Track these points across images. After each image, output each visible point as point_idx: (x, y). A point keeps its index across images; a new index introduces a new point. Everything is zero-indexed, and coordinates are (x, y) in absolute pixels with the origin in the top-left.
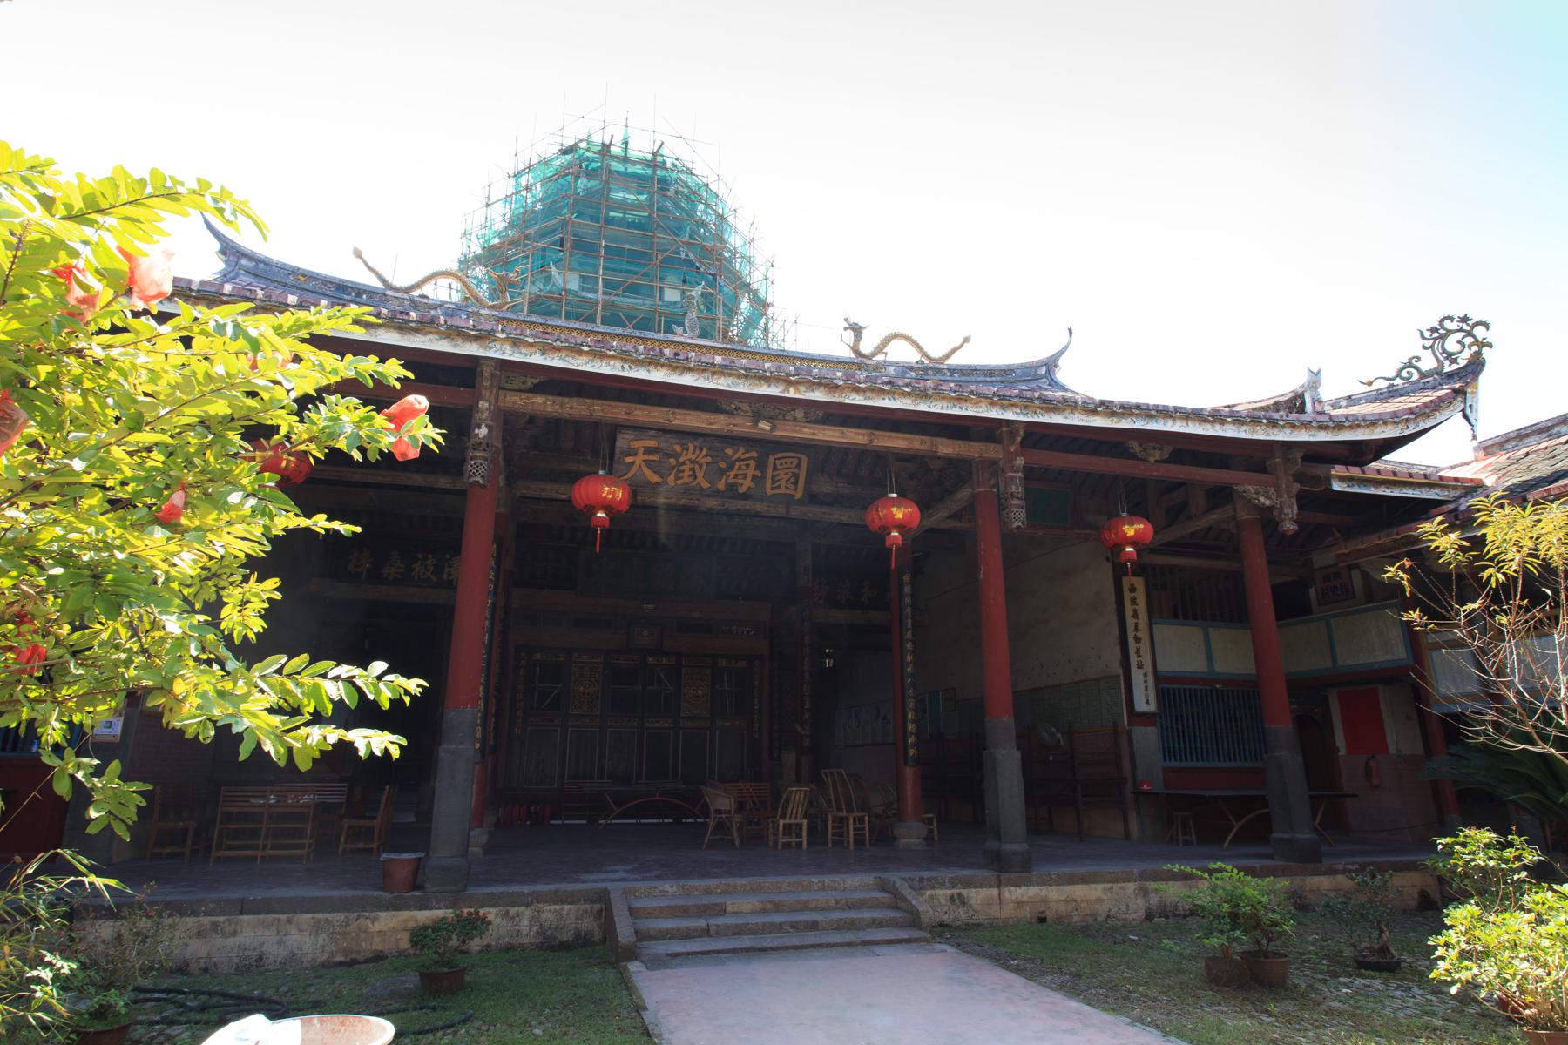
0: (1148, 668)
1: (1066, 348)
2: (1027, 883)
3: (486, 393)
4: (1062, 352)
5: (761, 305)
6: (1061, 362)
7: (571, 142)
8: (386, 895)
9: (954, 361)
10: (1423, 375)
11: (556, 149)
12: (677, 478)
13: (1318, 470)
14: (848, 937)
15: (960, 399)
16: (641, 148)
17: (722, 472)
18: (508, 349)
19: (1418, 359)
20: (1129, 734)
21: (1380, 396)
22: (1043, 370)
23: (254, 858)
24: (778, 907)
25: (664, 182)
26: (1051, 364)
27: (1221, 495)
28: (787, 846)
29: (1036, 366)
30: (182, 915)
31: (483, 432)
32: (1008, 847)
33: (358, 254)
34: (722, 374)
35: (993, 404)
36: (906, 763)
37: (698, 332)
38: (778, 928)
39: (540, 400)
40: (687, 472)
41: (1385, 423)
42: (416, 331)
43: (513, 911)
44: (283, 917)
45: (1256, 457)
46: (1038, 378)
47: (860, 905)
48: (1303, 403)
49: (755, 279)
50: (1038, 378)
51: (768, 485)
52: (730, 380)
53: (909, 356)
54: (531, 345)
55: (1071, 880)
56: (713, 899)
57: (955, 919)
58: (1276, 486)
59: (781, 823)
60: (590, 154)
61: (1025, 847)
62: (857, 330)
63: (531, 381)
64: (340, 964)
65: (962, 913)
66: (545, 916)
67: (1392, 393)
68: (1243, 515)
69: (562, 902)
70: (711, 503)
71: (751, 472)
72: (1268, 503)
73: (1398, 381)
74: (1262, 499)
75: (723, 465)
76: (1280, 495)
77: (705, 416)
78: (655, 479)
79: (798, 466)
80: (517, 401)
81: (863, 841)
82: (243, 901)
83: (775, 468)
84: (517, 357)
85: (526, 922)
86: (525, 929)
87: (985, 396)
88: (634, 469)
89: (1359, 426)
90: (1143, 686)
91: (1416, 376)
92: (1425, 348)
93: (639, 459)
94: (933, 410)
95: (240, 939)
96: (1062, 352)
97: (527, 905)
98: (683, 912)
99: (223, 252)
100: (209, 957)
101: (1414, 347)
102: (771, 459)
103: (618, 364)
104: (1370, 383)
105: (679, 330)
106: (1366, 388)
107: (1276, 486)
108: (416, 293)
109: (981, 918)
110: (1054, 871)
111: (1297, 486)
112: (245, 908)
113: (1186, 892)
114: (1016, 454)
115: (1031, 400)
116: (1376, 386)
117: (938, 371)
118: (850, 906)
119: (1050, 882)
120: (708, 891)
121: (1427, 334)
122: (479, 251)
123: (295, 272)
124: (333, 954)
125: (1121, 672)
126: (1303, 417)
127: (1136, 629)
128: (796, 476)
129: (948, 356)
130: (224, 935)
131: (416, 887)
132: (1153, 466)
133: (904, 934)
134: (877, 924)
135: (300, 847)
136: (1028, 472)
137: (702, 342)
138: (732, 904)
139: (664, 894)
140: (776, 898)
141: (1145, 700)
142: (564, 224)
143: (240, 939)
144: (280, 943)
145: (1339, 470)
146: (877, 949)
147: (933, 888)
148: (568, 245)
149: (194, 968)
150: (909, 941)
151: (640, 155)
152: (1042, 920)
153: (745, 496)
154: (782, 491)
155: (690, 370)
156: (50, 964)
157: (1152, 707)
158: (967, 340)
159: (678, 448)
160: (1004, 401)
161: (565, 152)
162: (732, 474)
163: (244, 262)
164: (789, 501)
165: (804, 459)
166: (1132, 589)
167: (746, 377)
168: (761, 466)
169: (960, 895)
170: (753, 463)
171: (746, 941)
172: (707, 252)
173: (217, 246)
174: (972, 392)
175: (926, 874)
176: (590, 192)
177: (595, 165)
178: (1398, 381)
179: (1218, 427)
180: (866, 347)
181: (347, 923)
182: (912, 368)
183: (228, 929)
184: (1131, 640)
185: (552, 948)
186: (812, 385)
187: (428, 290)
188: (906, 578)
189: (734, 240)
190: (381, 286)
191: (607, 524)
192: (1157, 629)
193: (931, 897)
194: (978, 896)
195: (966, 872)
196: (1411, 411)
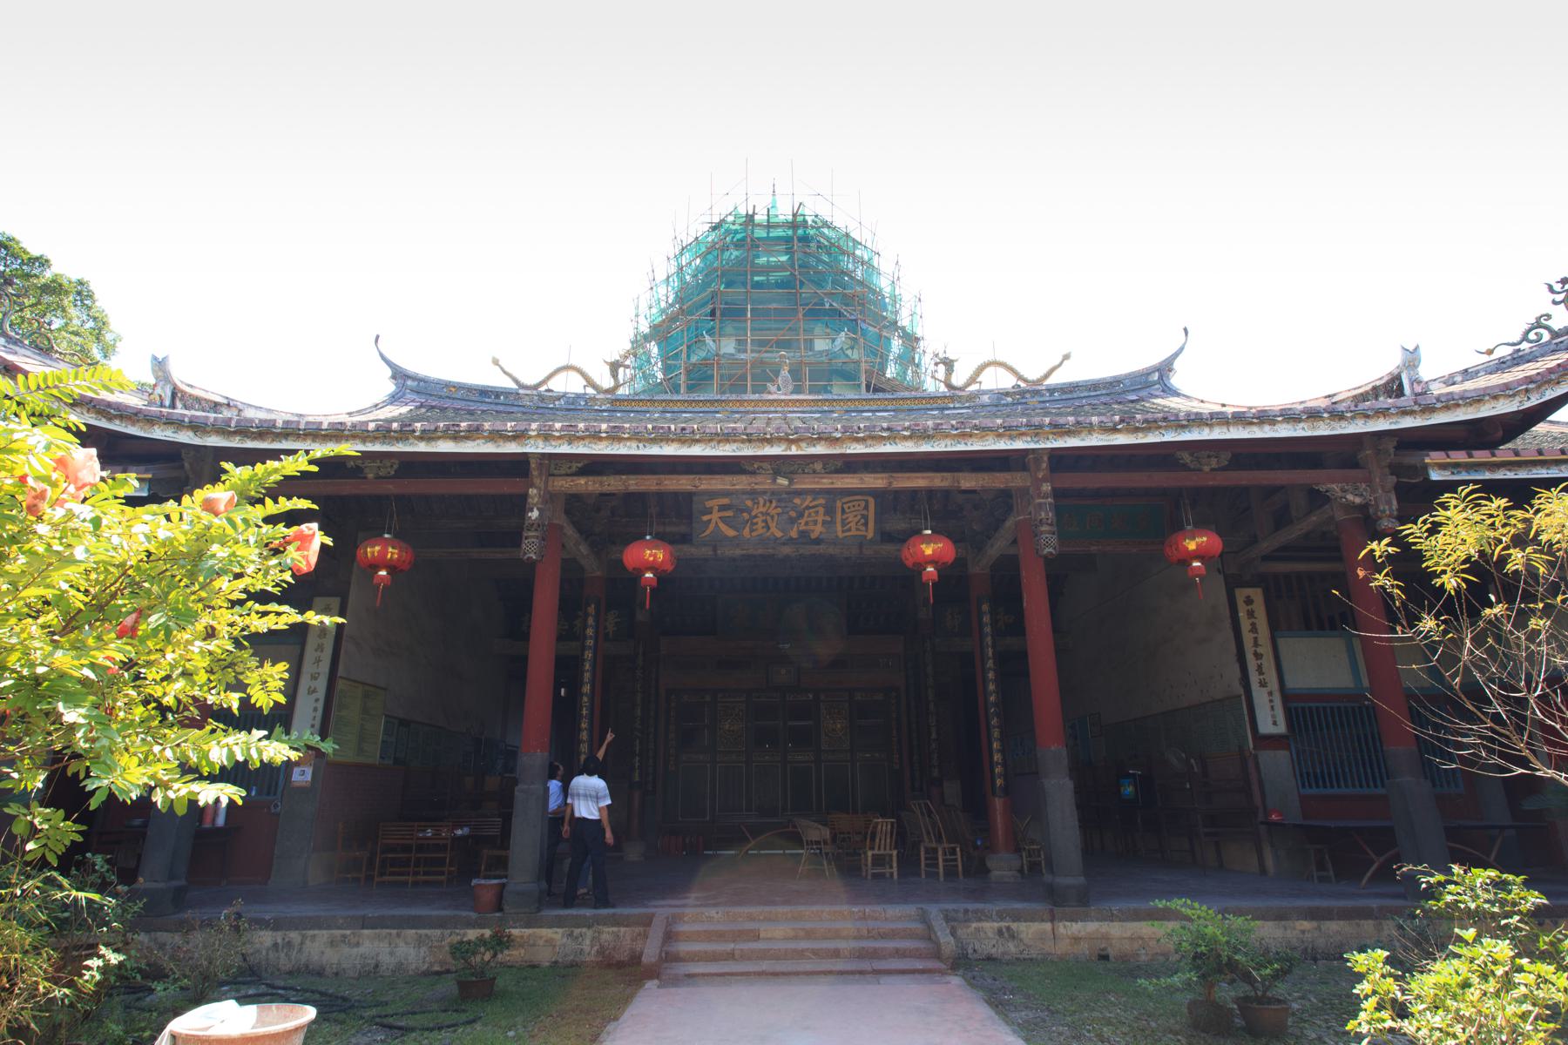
0: (1274, 684)
1: (1182, 349)
2: (1085, 918)
3: (537, 481)
4: (1176, 355)
5: (911, 340)
6: (1177, 364)
7: (716, 220)
8: (473, 915)
9: (1053, 380)
10: (1555, 334)
11: (707, 227)
12: (752, 531)
13: (1411, 459)
14: (867, 965)
15: (964, 435)
16: (784, 213)
17: (792, 521)
18: (540, 443)
19: (1549, 317)
20: (1256, 757)
21: (1502, 365)
22: (1156, 377)
23: (406, 883)
24: (809, 935)
25: (805, 240)
26: (1165, 368)
27: (1318, 499)
28: (875, 876)
29: (1147, 373)
30: (320, 928)
31: (535, 514)
32: (1063, 881)
33: (496, 362)
34: (728, 441)
35: (1000, 436)
36: (994, 794)
37: (791, 388)
38: (800, 954)
39: (582, 481)
40: (761, 525)
41: (1495, 398)
42: (466, 438)
43: (577, 931)
44: (394, 932)
45: (1343, 454)
46: (1149, 385)
47: (892, 935)
48: (1401, 385)
49: (904, 321)
50: (1149, 385)
51: (839, 528)
52: (734, 446)
53: (1006, 382)
54: (559, 438)
55: (1137, 916)
56: (749, 926)
57: (1003, 954)
58: (1369, 481)
59: (870, 853)
60: (737, 227)
61: (1082, 880)
62: (949, 364)
63: (575, 466)
64: (438, 973)
65: (1012, 947)
66: (605, 937)
67: (1518, 359)
68: (1340, 516)
69: (618, 924)
70: (787, 550)
71: (820, 519)
72: (1358, 500)
73: (1525, 346)
74: (1350, 497)
75: (793, 514)
76: (1373, 491)
77: (728, 478)
78: (731, 533)
79: (866, 508)
80: (563, 484)
81: (957, 874)
82: (364, 917)
83: (843, 511)
84: (549, 450)
85: (588, 942)
86: (587, 948)
87: (990, 429)
88: (712, 526)
89: (1458, 405)
90: (1268, 705)
91: (1546, 336)
92: (1555, 303)
93: (715, 516)
94: (937, 449)
95: (361, 950)
96: (1176, 355)
97: (589, 927)
98: (720, 936)
99: (394, 377)
100: (339, 964)
101: (1542, 303)
102: (839, 504)
103: (634, 444)
104: (1490, 352)
105: (773, 388)
106: (1485, 358)
107: (1369, 481)
108: (543, 389)
109: (1034, 953)
110: (1116, 907)
111: (1394, 479)
112: (365, 923)
113: (1279, 933)
114: (1045, 480)
115: (1041, 426)
116: (1496, 355)
117: (1037, 393)
118: (883, 936)
119: (1111, 918)
120: (751, 918)
121: (1558, 287)
122: (647, 331)
123: (448, 385)
124: (431, 964)
125: (1242, 691)
126: (1402, 402)
127: (1256, 644)
128: (865, 517)
129: (1047, 376)
130: (351, 945)
131: (499, 908)
132: (1209, 474)
133: (919, 965)
134: (899, 954)
135: (442, 873)
136: (1058, 494)
137: (795, 397)
138: (766, 930)
139: (710, 919)
140: (808, 926)
141: (1271, 720)
142: (714, 295)
143: (361, 950)
144: (392, 954)
145: (1436, 457)
146: (884, 979)
147: (980, 920)
148: (718, 313)
149: (328, 971)
150: (922, 972)
151: (781, 218)
152: (1104, 957)
153: (818, 541)
154: (854, 532)
155: (698, 441)
156: (103, 956)
157: (1281, 728)
158: (1066, 357)
159: (749, 503)
160: (1009, 431)
161: (714, 228)
162: (802, 521)
163: (409, 383)
164: (861, 543)
165: (871, 501)
166: (1249, 601)
167: (750, 441)
168: (830, 511)
169: (1008, 928)
170: (821, 510)
171: (765, 966)
172: (848, 300)
173: (389, 372)
174: (975, 427)
175: (971, 906)
176: (740, 262)
177: (739, 236)
178: (1525, 346)
179: (1267, 427)
180: (958, 379)
181: (443, 938)
182: (1007, 394)
183: (353, 940)
184: (1250, 657)
185: (609, 966)
186: (812, 442)
187: (552, 385)
188: (985, 607)
189: (883, 284)
190: (514, 386)
191: (655, 584)
192: (1281, 642)
193: (978, 930)
194: (1029, 931)
195: (1018, 906)
196: (1529, 380)
